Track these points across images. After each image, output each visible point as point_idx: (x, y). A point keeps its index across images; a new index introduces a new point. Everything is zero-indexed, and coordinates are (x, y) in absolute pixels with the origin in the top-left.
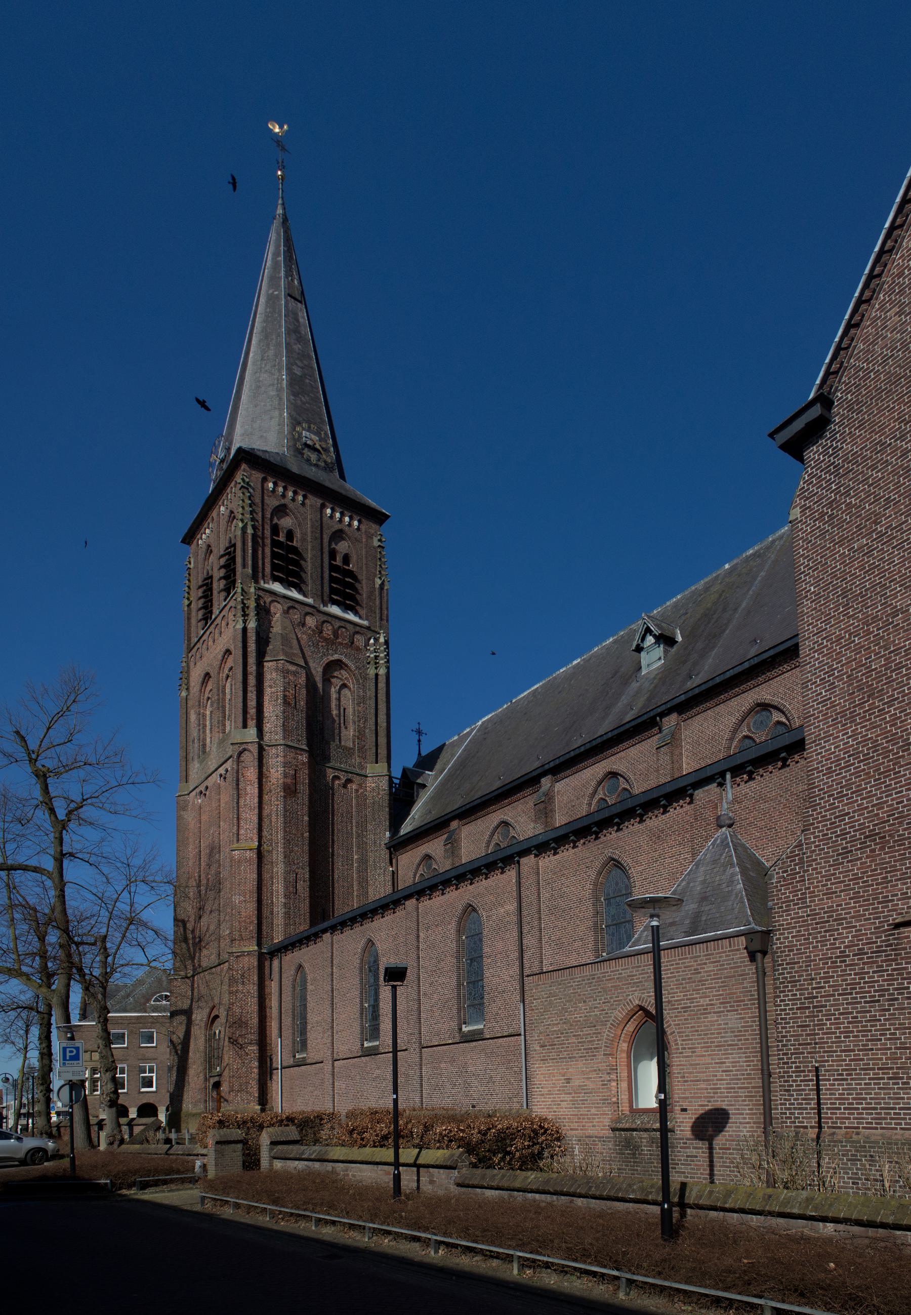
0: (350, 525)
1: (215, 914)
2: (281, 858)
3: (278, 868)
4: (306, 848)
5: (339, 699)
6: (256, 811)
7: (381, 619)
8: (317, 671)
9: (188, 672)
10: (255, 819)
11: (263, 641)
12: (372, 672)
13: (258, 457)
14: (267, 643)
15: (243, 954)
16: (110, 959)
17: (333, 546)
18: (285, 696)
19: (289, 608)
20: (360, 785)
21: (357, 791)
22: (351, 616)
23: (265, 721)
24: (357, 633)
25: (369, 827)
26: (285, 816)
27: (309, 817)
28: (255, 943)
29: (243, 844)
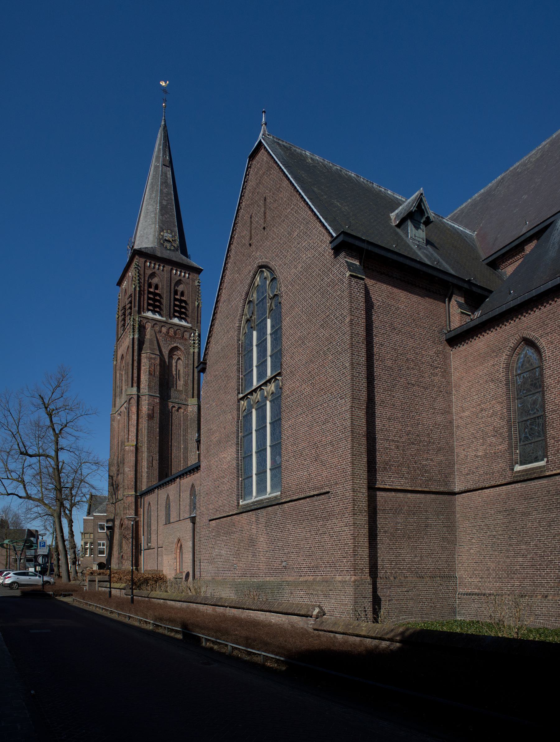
0: (184, 276)
1: (122, 475)
2: (146, 449)
3: (144, 455)
4: (157, 444)
5: (176, 366)
6: (136, 427)
7: (197, 323)
8: (166, 352)
9: (117, 352)
10: (135, 431)
11: (141, 343)
12: (192, 351)
13: (142, 252)
14: (143, 343)
15: (129, 496)
16: (73, 498)
17: (176, 288)
18: (149, 370)
19: (154, 325)
20: (185, 410)
21: (183, 413)
22: (183, 323)
23: (141, 383)
24: (186, 331)
25: (189, 431)
26: (148, 429)
27: (159, 429)
28: (134, 490)
29: (130, 443)
